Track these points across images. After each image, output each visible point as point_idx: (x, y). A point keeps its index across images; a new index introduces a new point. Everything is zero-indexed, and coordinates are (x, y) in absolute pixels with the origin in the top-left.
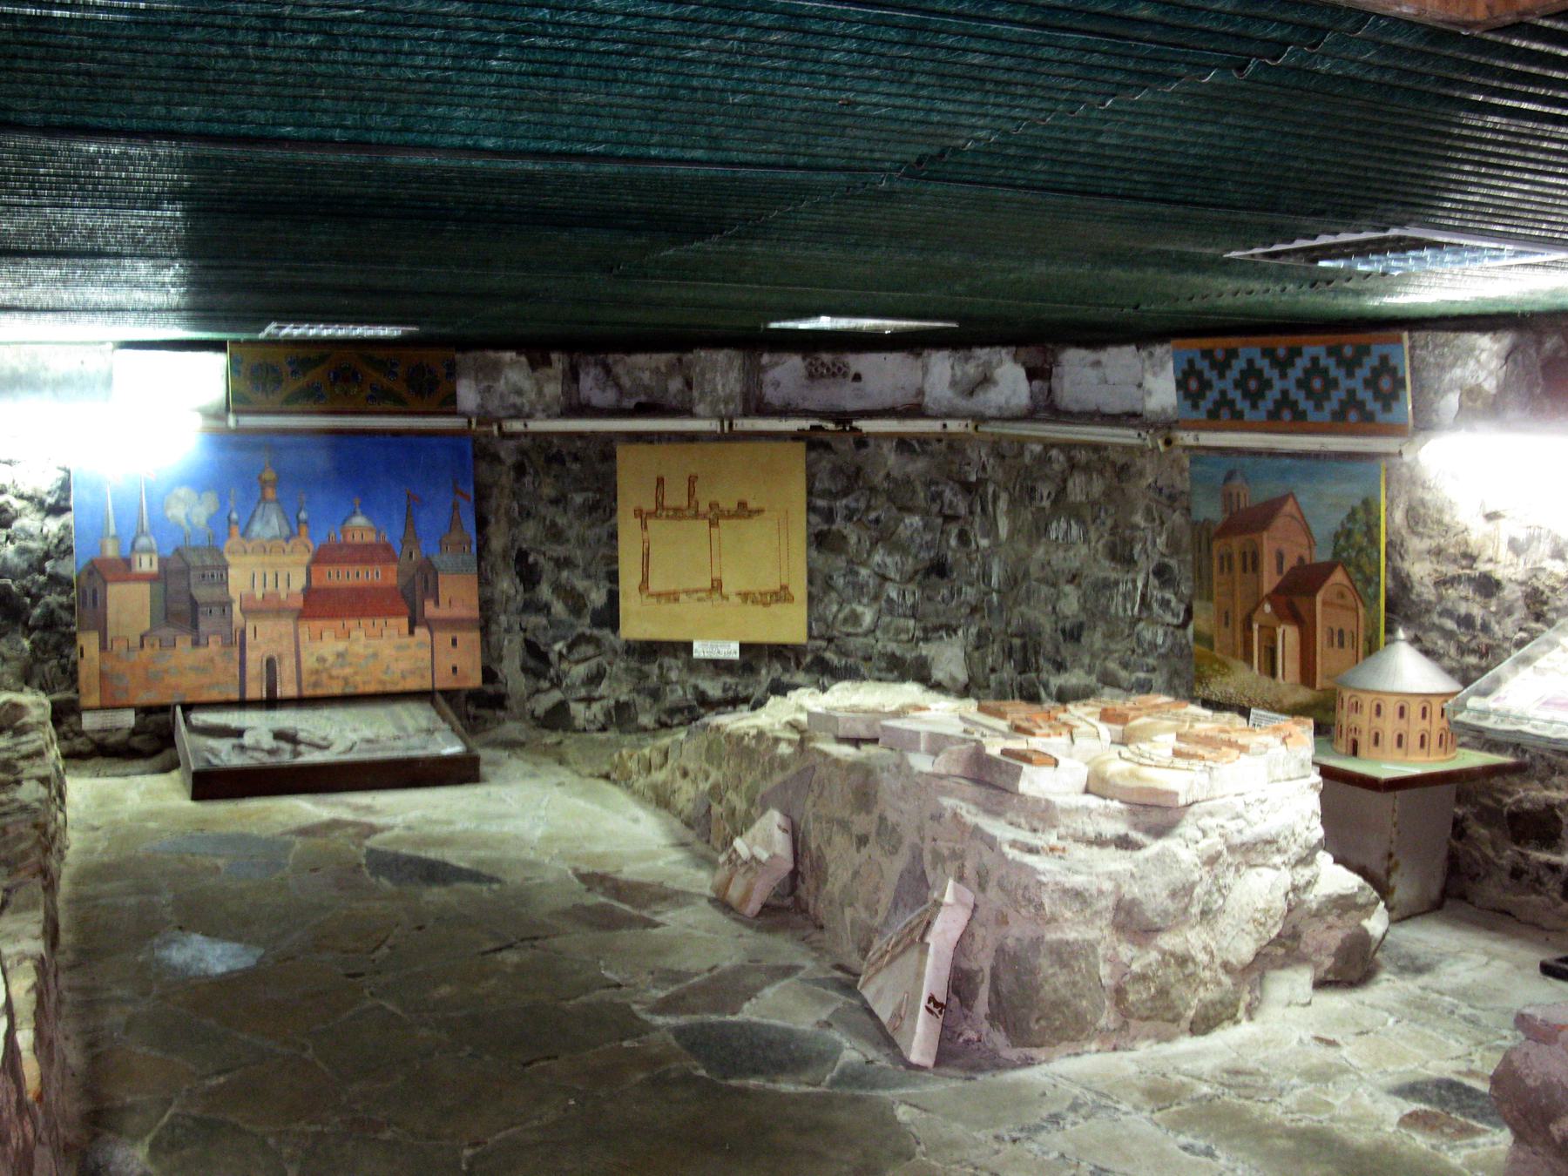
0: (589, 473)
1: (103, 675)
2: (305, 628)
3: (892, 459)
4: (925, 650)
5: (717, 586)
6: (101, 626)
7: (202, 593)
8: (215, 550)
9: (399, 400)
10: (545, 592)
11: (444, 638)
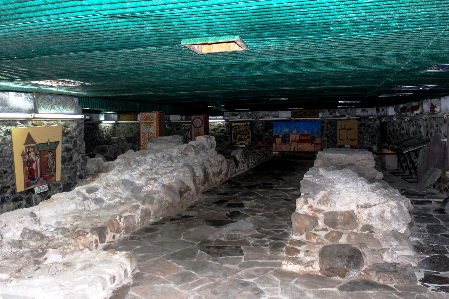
1: (275, 148)
4: (372, 146)
5: (348, 138)
6: (275, 142)
7: (287, 139)
9: (311, 116)
11: (316, 145)
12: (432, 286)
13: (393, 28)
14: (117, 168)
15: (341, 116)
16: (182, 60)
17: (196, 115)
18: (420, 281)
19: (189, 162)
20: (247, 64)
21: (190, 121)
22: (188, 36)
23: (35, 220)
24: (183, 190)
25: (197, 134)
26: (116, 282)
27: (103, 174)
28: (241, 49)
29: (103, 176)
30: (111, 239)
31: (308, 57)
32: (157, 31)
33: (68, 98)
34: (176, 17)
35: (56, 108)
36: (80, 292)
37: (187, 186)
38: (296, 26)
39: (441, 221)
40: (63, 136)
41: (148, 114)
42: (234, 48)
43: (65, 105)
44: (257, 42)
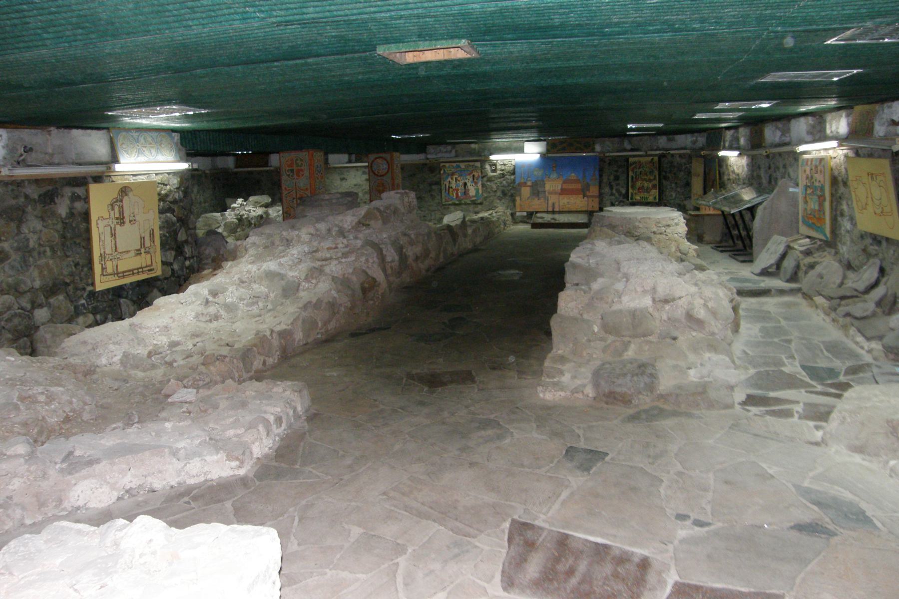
0: (433, 168)
2: (561, 197)
3: (678, 159)
6: (520, 195)
7: (540, 189)
8: (543, 181)
10: (614, 191)
11: (591, 199)
12: (754, 410)
13: (694, 30)
14: (252, 251)
15: (632, 150)
16: (371, 72)
17: (377, 153)
18: (740, 404)
19: (374, 238)
20: (475, 74)
21: (366, 164)
22: (387, 41)
23: (137, 338)
24: (367, 286)
25: (381, 188)
26: (284, 426)
27: (230, 263)
28: (469, 56)
29: (231, 267)
30: (261, 366)
31: (573, 63)
32: (342, 37)
33: (163, 134)
34: (374, 20)
35: (147, 153)
36: (235, 439)
37: (373, 278)
38: (553, 27)
39: (781, 320)
40: (160, 200)
41: (293, 155)
42: (458, 54)
43: (158, 145)
44: (494, 46)
